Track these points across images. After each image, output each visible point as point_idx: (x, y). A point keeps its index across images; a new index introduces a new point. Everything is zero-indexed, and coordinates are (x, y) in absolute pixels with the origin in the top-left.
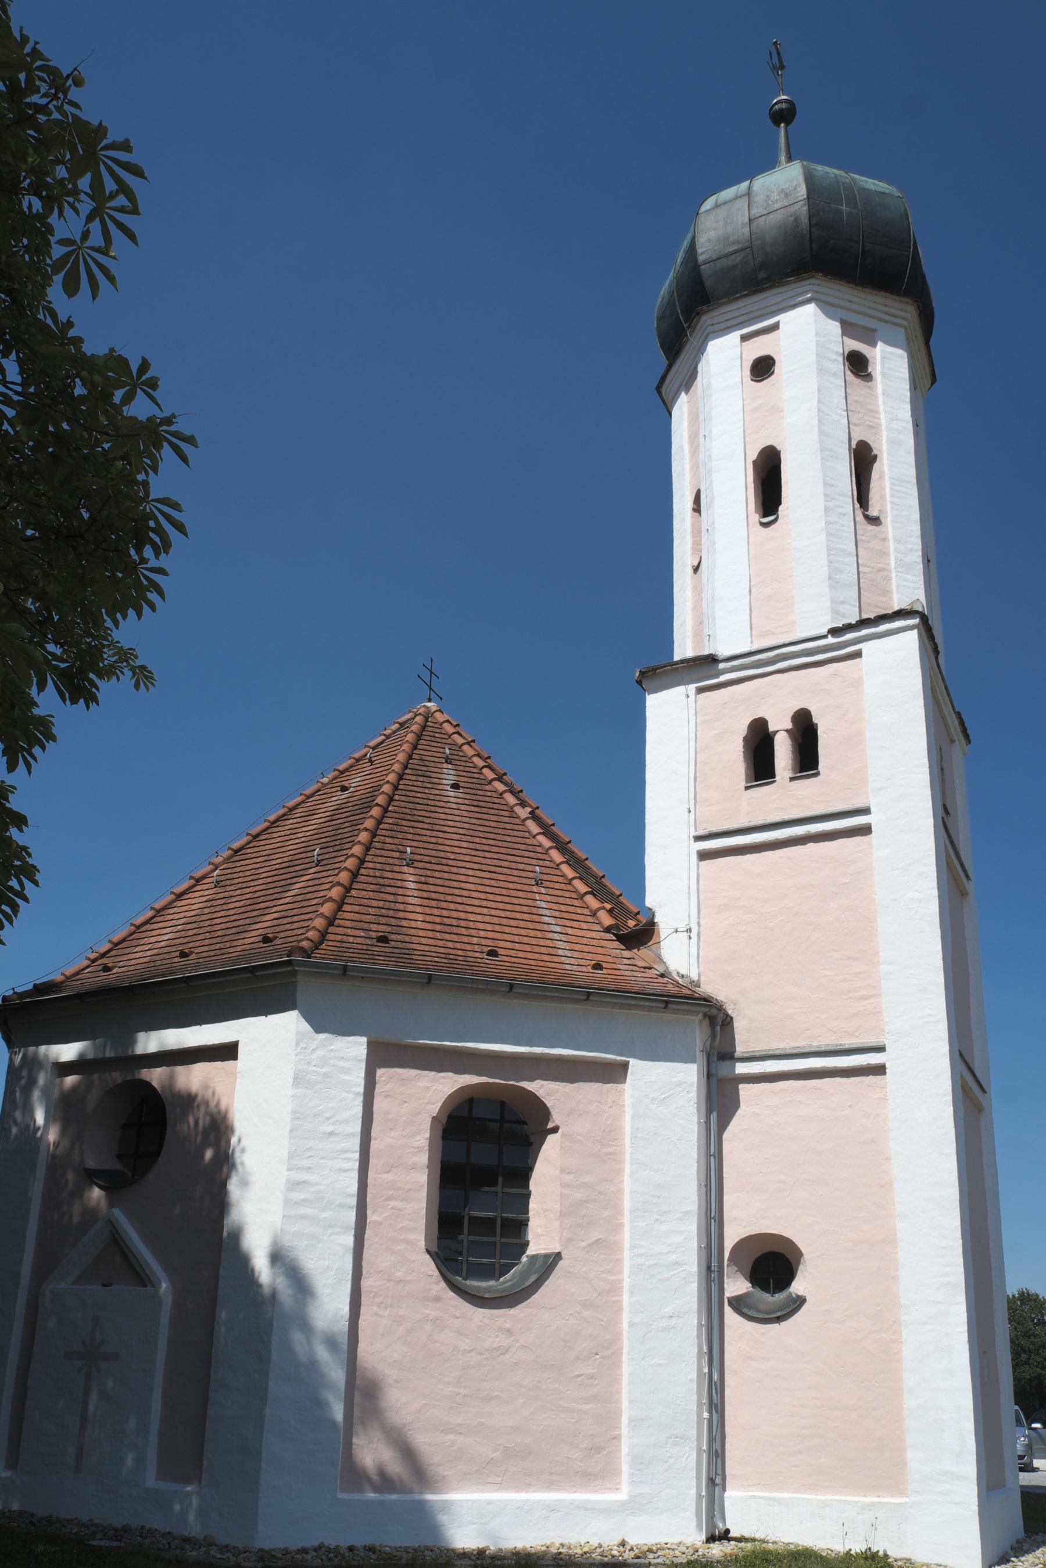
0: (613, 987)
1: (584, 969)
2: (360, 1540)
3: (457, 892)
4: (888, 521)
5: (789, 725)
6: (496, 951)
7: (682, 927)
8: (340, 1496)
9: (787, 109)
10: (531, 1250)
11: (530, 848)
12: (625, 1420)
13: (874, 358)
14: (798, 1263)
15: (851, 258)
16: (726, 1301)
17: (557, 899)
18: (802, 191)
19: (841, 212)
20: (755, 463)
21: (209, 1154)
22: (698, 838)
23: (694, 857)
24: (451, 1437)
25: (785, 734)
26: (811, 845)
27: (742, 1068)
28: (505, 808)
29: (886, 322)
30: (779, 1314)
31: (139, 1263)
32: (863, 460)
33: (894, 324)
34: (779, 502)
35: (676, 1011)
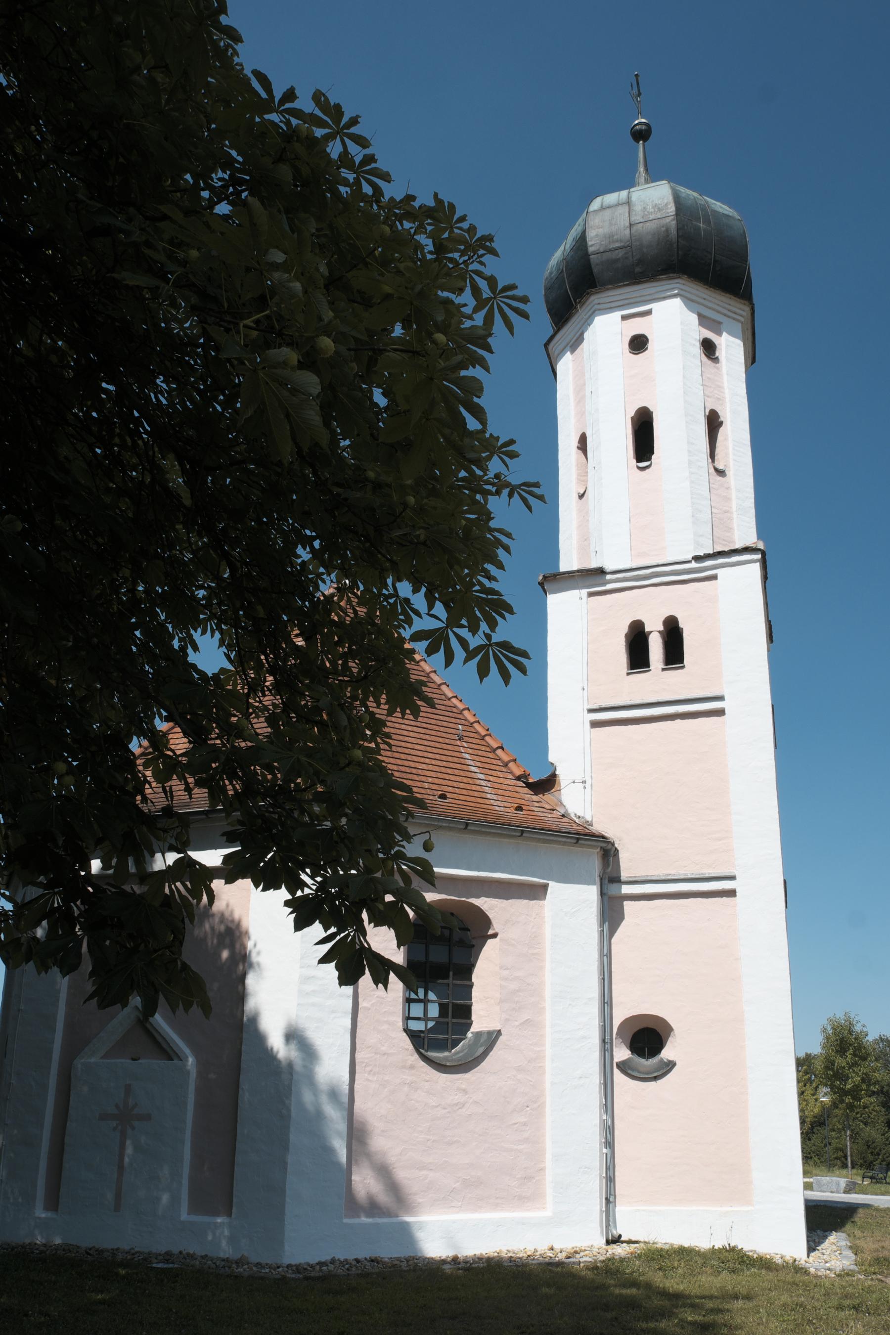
0: (537, 826)
1: (508, 810)
2: (363, 1254)
3: (403, 744)
4: (730, 473)
5: (661, 628)
6: (445, 795)
7: (579, 779)
8: (346, 1221)
9: (646, 130)
10: (475, 1028)
11: (448, 709)
12: (548, 1156)
13: (720, 345)
14: (669, 1036)
15: (703, 261)
16: (615, 1065)
17: (476, 752)
18: (672, 209)
19: (699, 228)
20: (632, 418)
21: (225, 954)
22: (591, 711)
23: (588, 725)
24: (425, 1172)
25: (658, 634)
26: (678, 721)
27: (626, 889)
28: (422, 674)
29: (729, 317)
30: (655, 1074)
31: (164, 1039)
32: (714, 423)
33: (734, 319)
34: (652, 452)
35: (583, 846)
